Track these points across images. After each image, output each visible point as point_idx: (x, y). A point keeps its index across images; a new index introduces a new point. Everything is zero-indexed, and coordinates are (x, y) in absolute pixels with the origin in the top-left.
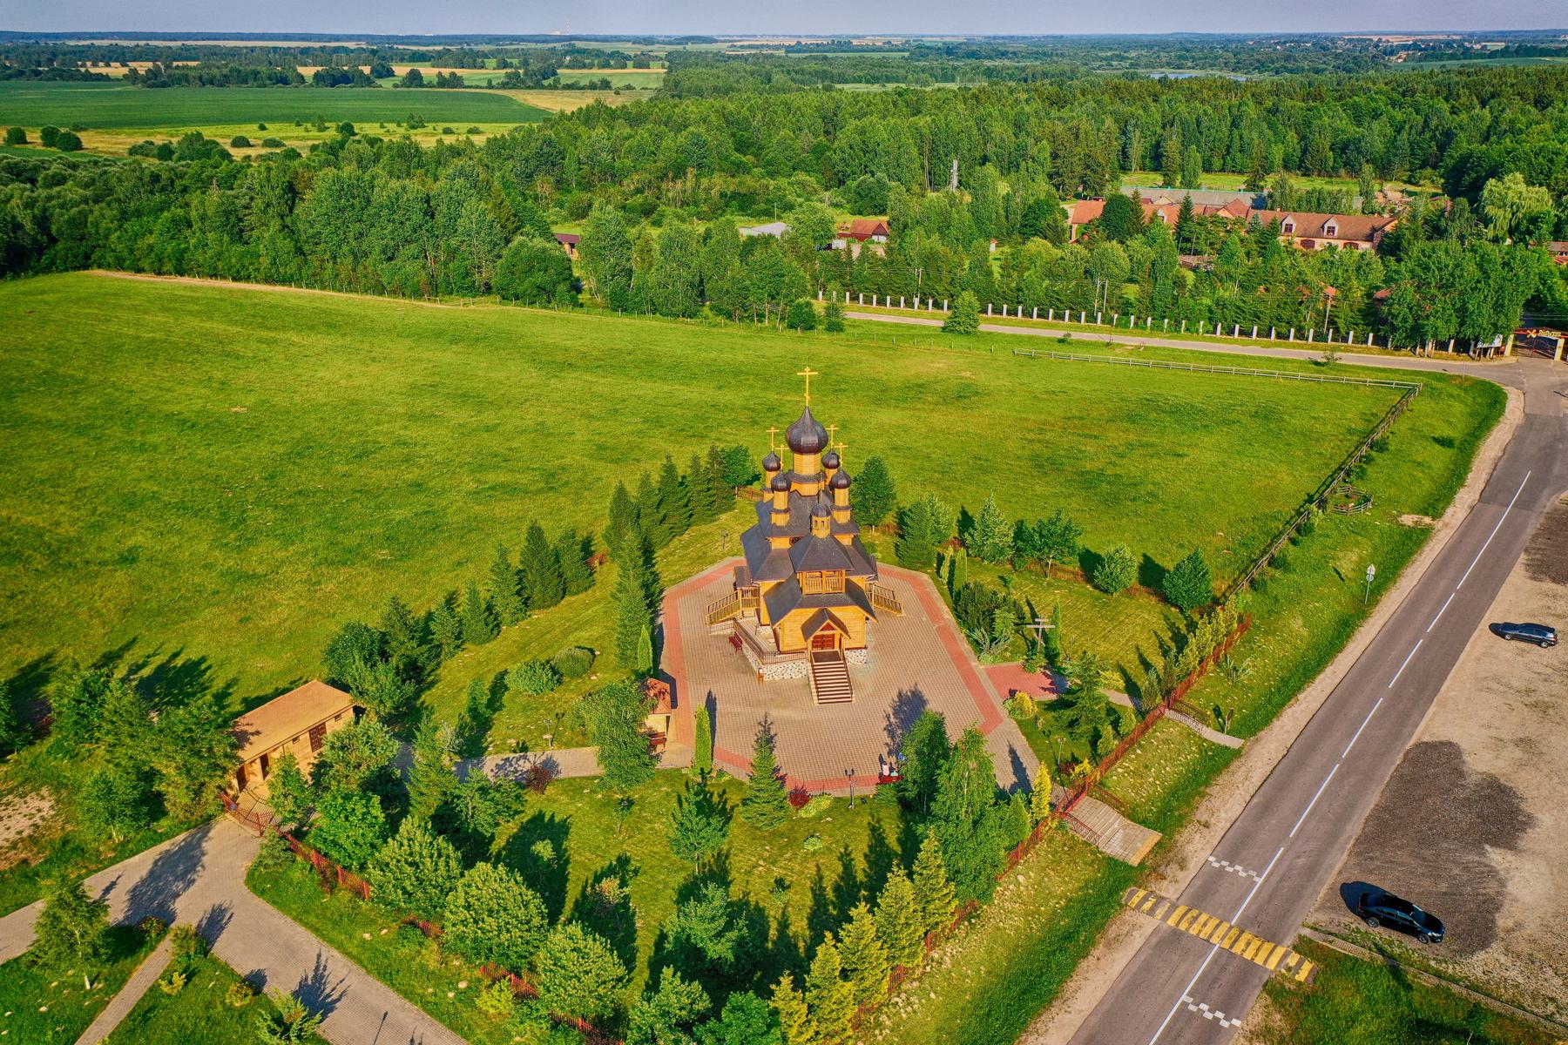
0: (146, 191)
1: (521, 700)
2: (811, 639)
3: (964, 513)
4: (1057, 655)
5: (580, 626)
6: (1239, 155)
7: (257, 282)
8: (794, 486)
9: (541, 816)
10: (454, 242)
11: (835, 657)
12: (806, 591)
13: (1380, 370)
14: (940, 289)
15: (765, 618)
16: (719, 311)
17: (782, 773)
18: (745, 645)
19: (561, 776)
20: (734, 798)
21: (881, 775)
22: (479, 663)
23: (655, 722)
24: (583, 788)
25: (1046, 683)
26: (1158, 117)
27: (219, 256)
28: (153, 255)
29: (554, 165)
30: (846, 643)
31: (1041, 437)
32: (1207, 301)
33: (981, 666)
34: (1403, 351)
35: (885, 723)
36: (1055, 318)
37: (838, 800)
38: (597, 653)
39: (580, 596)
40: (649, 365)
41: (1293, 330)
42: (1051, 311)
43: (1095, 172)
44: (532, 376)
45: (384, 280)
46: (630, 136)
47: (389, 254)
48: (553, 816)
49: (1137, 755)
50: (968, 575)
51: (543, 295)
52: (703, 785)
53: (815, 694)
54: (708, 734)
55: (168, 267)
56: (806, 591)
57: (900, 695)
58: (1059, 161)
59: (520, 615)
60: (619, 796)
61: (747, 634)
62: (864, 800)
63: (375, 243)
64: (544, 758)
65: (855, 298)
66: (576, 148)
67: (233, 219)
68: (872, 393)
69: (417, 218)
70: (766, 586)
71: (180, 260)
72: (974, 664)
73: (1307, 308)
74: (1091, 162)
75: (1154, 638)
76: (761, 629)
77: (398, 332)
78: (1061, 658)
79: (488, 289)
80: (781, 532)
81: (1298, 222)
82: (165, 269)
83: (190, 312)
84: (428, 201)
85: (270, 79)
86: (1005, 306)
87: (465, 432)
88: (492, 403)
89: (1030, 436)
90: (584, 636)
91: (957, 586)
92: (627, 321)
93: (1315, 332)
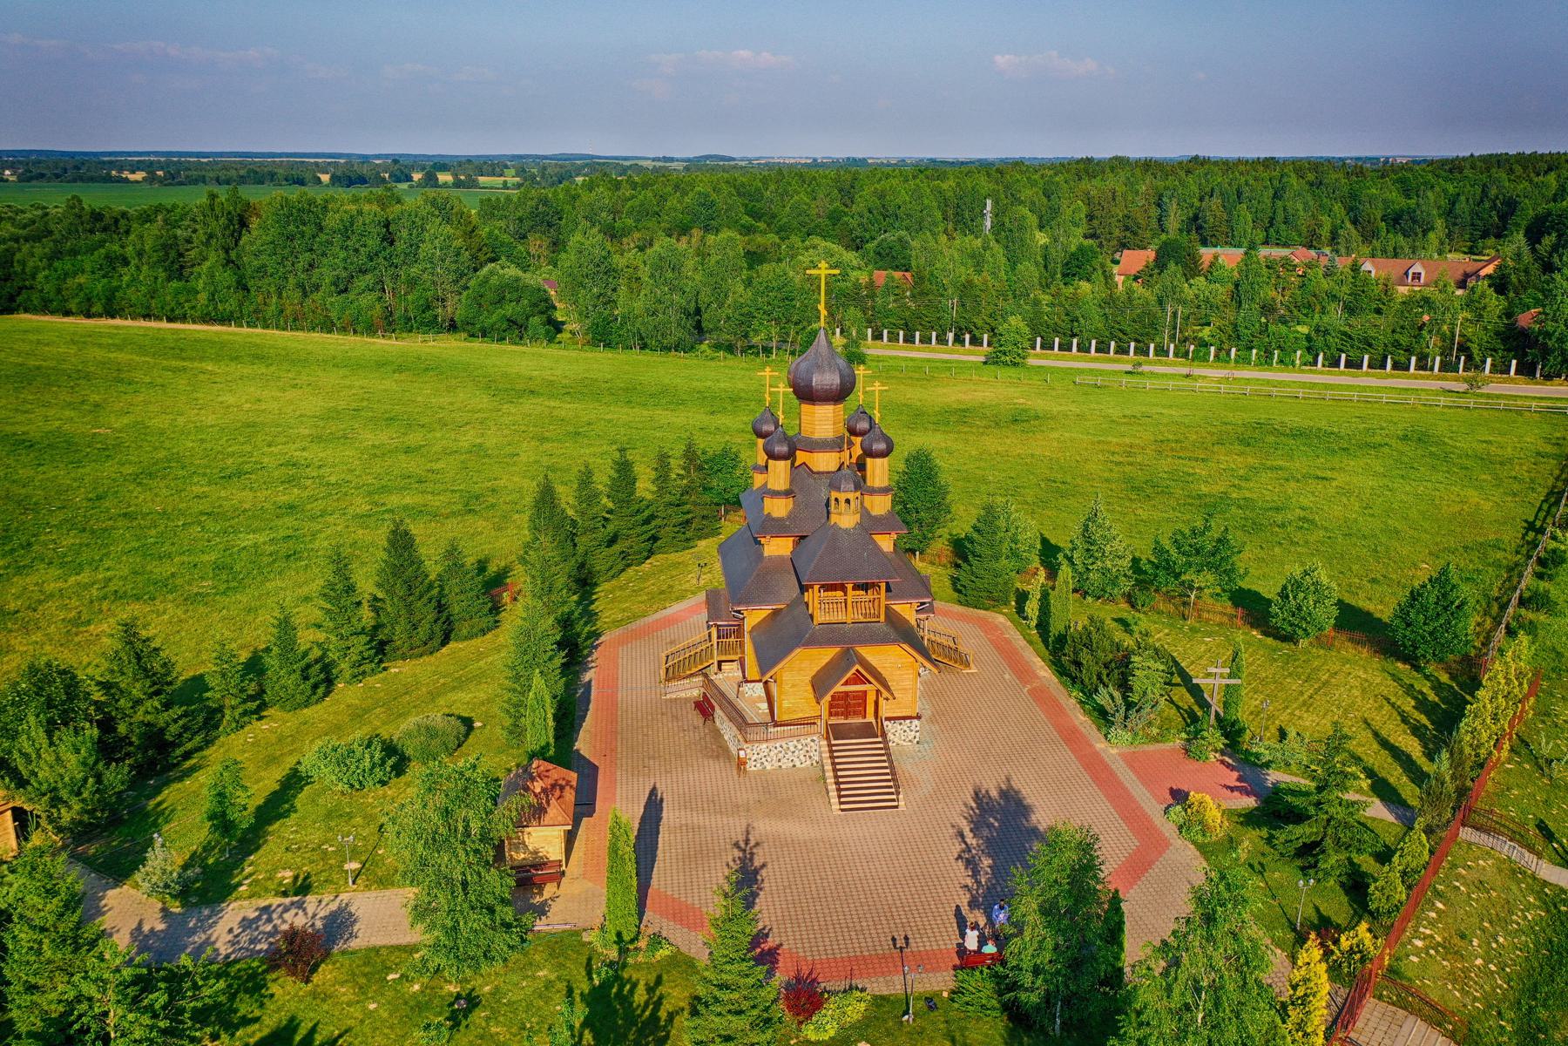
0: (85, 230)
1: (326, 802)
2: (828, 698)
3: (1044, 541)
4: (1241, 731)
5: (460, 684)
6: (1283, 227)
7: (194, 322)
8: (801, 456)
9: (292, 1025)
10: (414, 271)
11: (867, 731)
12: (820, 617)
13: (1541, 398)
14: (980, 323)
15: (753, 670)
16: (717, 347)
17: (771, 942)
18: (718, 712)
19: (354, 944)
20: (675, 996)
21: (961, 950)
22: (280, 740)
23: (544, 840)
24: (389, 970)
25: (1232, 778)
26: (1195, 188)
27: (153, 294)
28: (82, 294)
29: (550, 225)
30: (886, 709)
31: (1131, 459)
32: (1304, 330)
33: (1113, 748)
34: (1557, 380)
35: (958, 847)
36: (1116, 352)
37: (880, 1001)
38: (478, 724)
39: (474, 642)
40: (630, 394)
41: (1414, 359)
42: (1113, 344)
43: (1135, 234)
44: (483, 401)
45: (333, 315)
46: (633, 197)
47: (342, 287)
48: (313, 1030)
49: (1439, 912)
50: (1072, 615)
51: (515, 329)
52: (617, 966)
53: (833, 794)
54: (631, 867)
55: (97, 308)
56: (820, 617)
57: (977, 796)
58: (1095, 223)
59: (367, 667)
60: (453, 989)
61: (723, 695)
62: (931, 1002)
63: (326, 274)
64: (334, 907)
65: (878, 336)
66: (574, 208)
67: (173, 254)
68: (904, 417)
69: (373, 243)
70: (754, 617)
71: (110, 299)
72: (1100, 745)
73: (1430, 332)
74: (1130, 223)
75: (1387, 707)
76: (747, 688)
77: (332, 362)
78: (1247, 735)
79: (453, 327)
80: (776, 527)
81: (1377, 269)
82: (94, 310)
83: (100, 345)
84: (387, 225)
85: (286, 180)
86: (1057, 340)
87: (378, 453)
88: (423, 426)
89: (1117, 458)
90: (462, 702)
91: (1056, 627)
92: (610, 355)
93: (1441, 361)
